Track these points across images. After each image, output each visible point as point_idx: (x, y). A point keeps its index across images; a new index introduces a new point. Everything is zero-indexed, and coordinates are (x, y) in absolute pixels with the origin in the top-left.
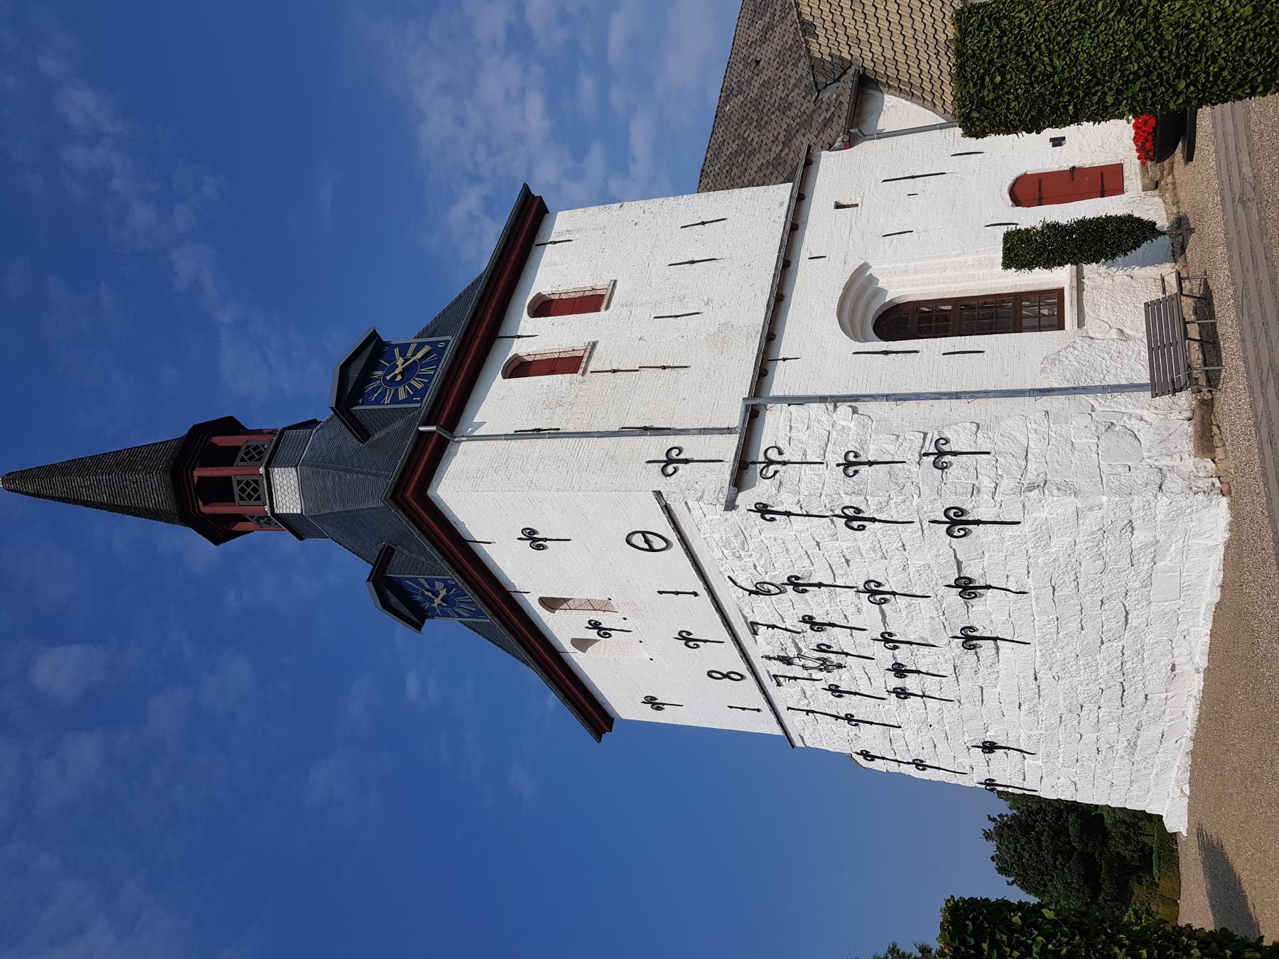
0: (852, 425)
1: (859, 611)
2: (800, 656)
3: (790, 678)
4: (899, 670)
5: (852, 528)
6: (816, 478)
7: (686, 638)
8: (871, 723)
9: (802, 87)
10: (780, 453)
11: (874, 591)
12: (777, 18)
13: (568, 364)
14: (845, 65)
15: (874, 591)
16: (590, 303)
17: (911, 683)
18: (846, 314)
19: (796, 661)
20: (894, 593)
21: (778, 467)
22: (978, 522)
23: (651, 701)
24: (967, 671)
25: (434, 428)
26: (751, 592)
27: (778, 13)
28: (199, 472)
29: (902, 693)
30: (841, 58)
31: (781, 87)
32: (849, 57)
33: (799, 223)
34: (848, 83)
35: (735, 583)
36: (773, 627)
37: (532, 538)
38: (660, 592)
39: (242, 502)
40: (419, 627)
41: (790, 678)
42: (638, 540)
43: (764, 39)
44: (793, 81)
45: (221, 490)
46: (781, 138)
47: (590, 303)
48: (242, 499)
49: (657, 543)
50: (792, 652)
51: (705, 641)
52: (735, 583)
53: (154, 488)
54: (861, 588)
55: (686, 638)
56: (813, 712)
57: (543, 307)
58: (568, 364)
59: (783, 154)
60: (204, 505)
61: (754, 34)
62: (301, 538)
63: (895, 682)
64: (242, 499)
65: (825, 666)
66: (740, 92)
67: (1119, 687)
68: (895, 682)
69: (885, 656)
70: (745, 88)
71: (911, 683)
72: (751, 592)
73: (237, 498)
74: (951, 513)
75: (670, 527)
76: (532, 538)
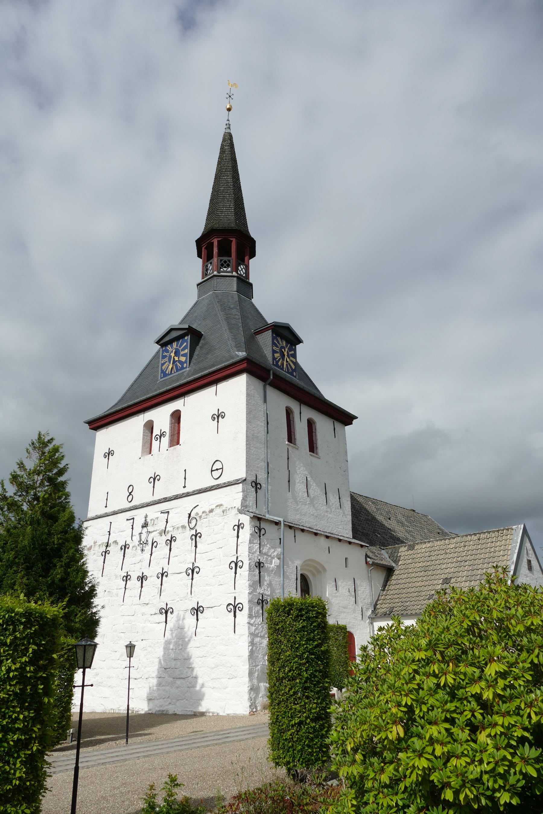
0: (273, 565)
1: (181, 563)
2: (149, 532)
3: (133, 526)
4: (142, 578)
5: (230, 564)
6: (255, 550)
7: (155, 479)
8: (104, 562)
9: (384, 542)
10: (263, 535)
11: (193, 571)
12: (407, 528)
13: (291, 438)
14: (396, 562)
15: (193, 571)
16: (312, 448)
17: (134, 583)
18: (310, 563)
19: (145, 530)
20: (192, 579)
21: (258, 534)
22: (235, 616)
23: (109, 454)
24: (146, 609)
25: (272, 378)
26: (190, 515)
27: (409, 529)
28: (234, 240)
29: (127, 578)
30: (399, 560)
31: (382, 531)
32: (399, 564)
33: (330, 539)
34: (388, 562)
35: (195, 508)
36: (167, 522)
37: (218, 416)
38: (185, 471)
39: (219, 260)
40: (157, 342)
41: (133, 526)
42: (218, 465)
43: (399, 522)
44: (385, 536)
45: (224, 251)
46: (365, 531)
47: (312, 448)
48: (221, 260)
49: (216, 474)
50: (150, 528)
51: (154, 487)
52: (195, 508)
53: (228, 219)
54: (196, 565)
55: (155, 479)
56: (109, 534)
57: (311, 424)
58: (291, 438)
59: (359, 532)
60: (218, 241)
61: (400, 517)
62: (198, 285)
63: (134, 576)
64: (221, 260)
65: (143, 543)
66: (378, 509)
67: (138, 676)
68: (134, 576)
69: (152, 572)
70: (379, 512)
71: (134, 583)
72: (190, 515)
73: (221, 258)
74: (240, 605)
75: (226, 481)
76: (218, 416)
